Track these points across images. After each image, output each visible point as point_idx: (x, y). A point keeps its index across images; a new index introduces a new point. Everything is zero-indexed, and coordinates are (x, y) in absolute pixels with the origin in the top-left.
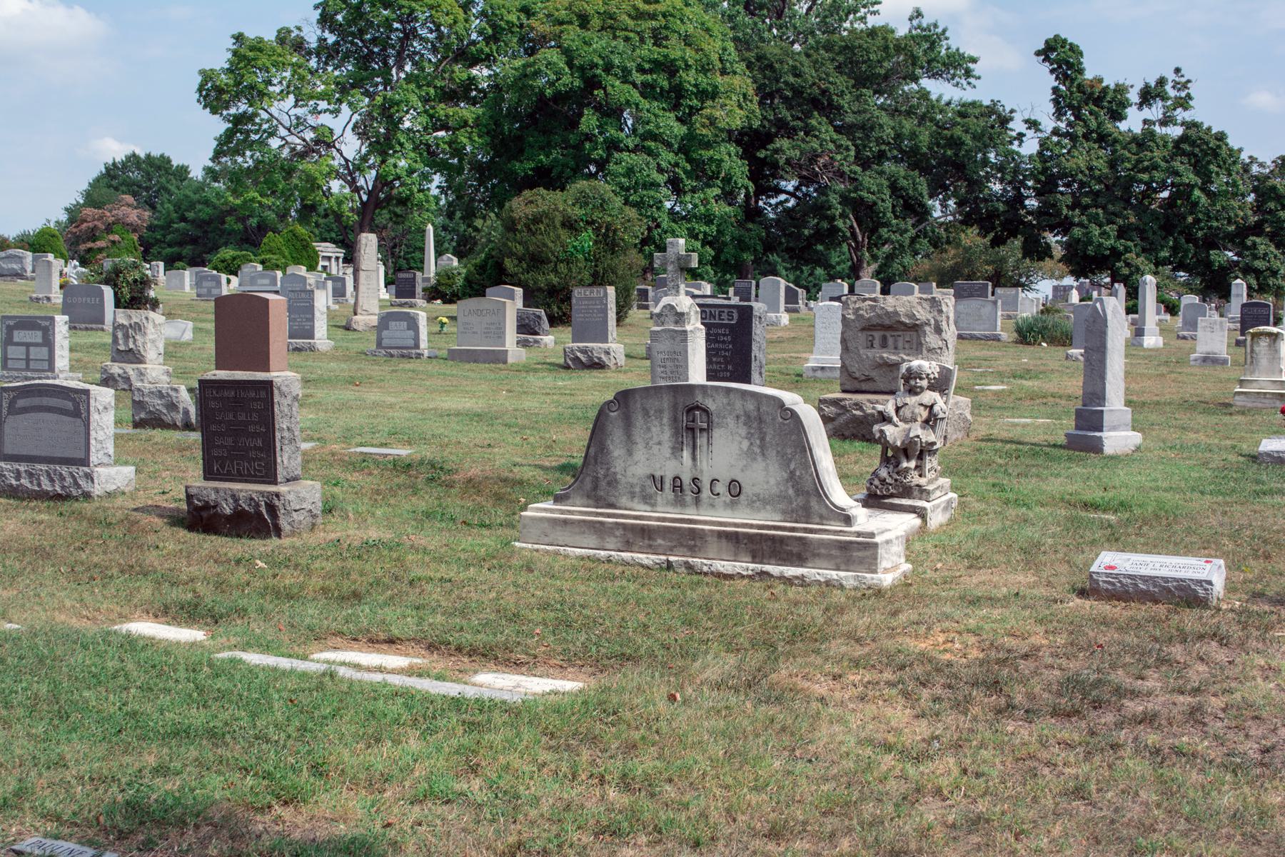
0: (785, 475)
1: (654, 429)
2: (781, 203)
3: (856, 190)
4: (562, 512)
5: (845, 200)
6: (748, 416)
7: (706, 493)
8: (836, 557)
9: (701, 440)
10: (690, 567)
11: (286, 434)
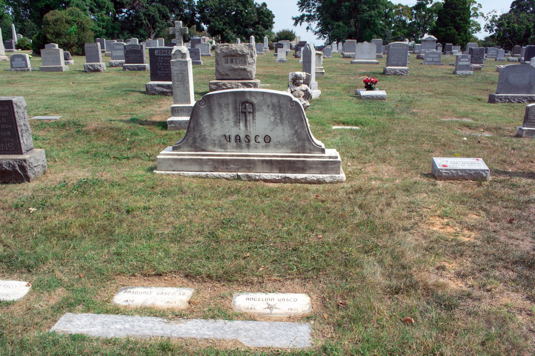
0: (293, 132)
1: (224, 113)
2: (123, 16)
3: (148, 11)
4: (179, 155)
5: (145, 14)
6: (273, 105)
7: (253, 142)
8: (321, 168)
9: (250, 118)
10: (249, 179)
11: (23, 128)
